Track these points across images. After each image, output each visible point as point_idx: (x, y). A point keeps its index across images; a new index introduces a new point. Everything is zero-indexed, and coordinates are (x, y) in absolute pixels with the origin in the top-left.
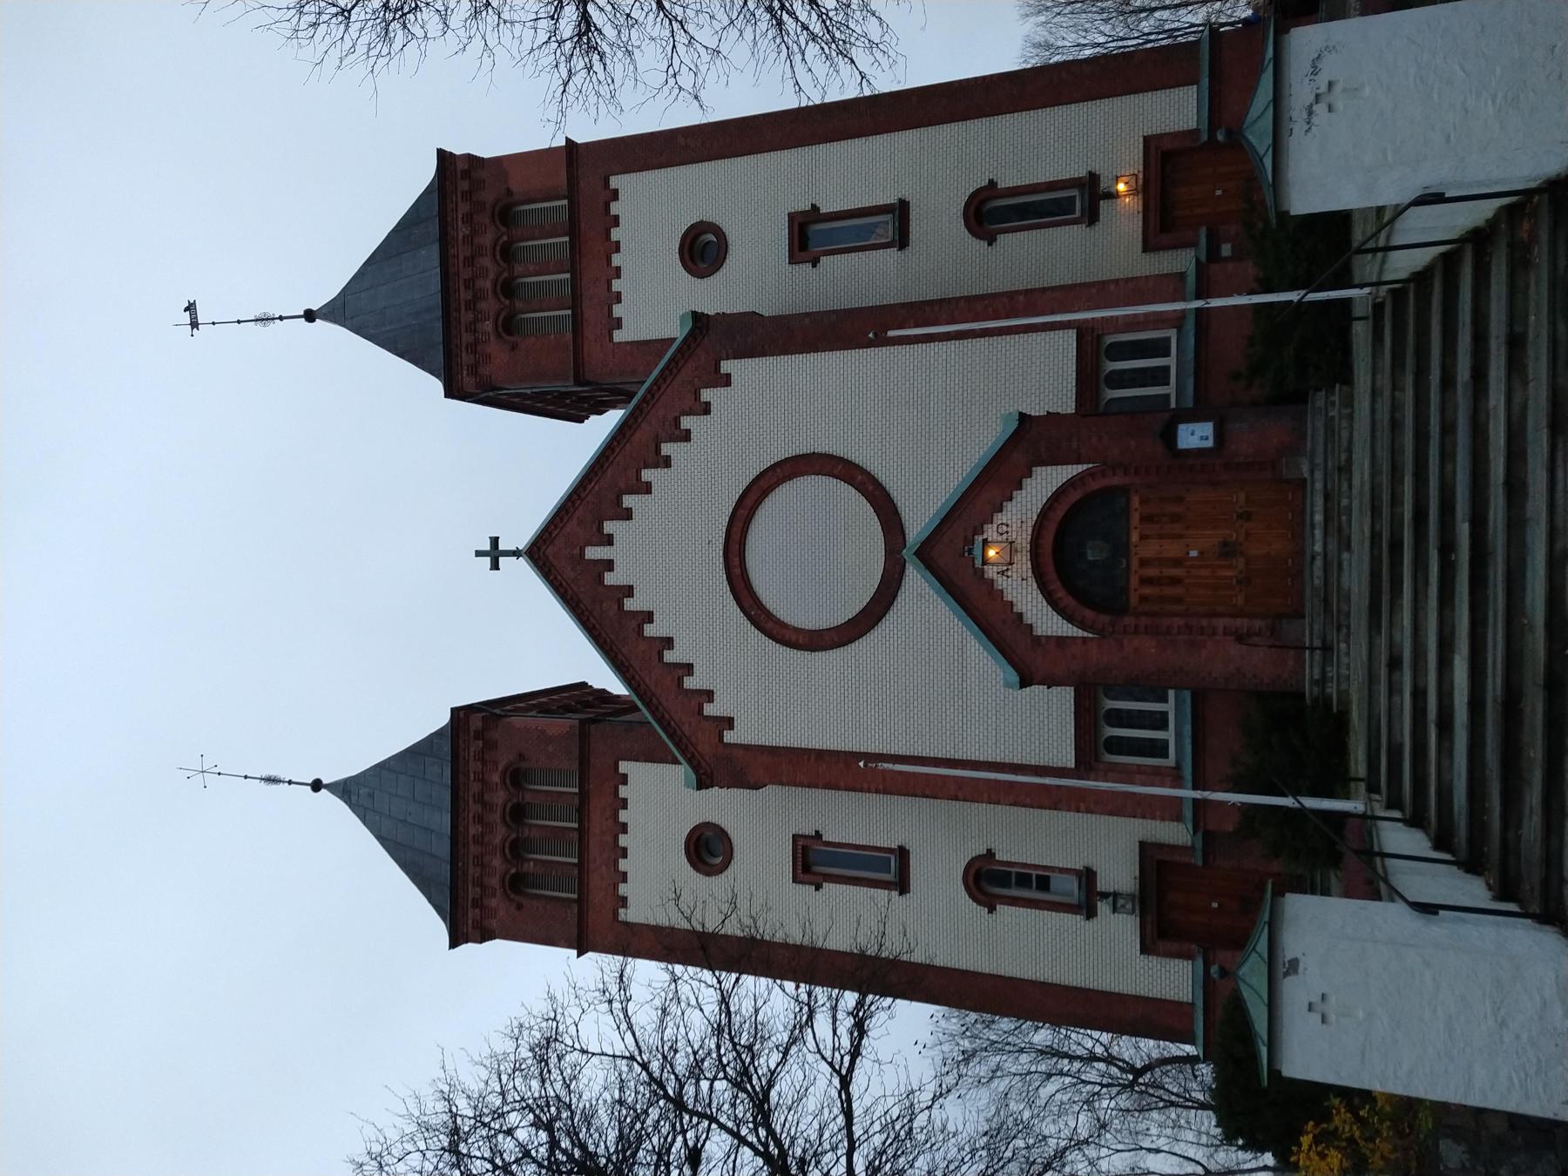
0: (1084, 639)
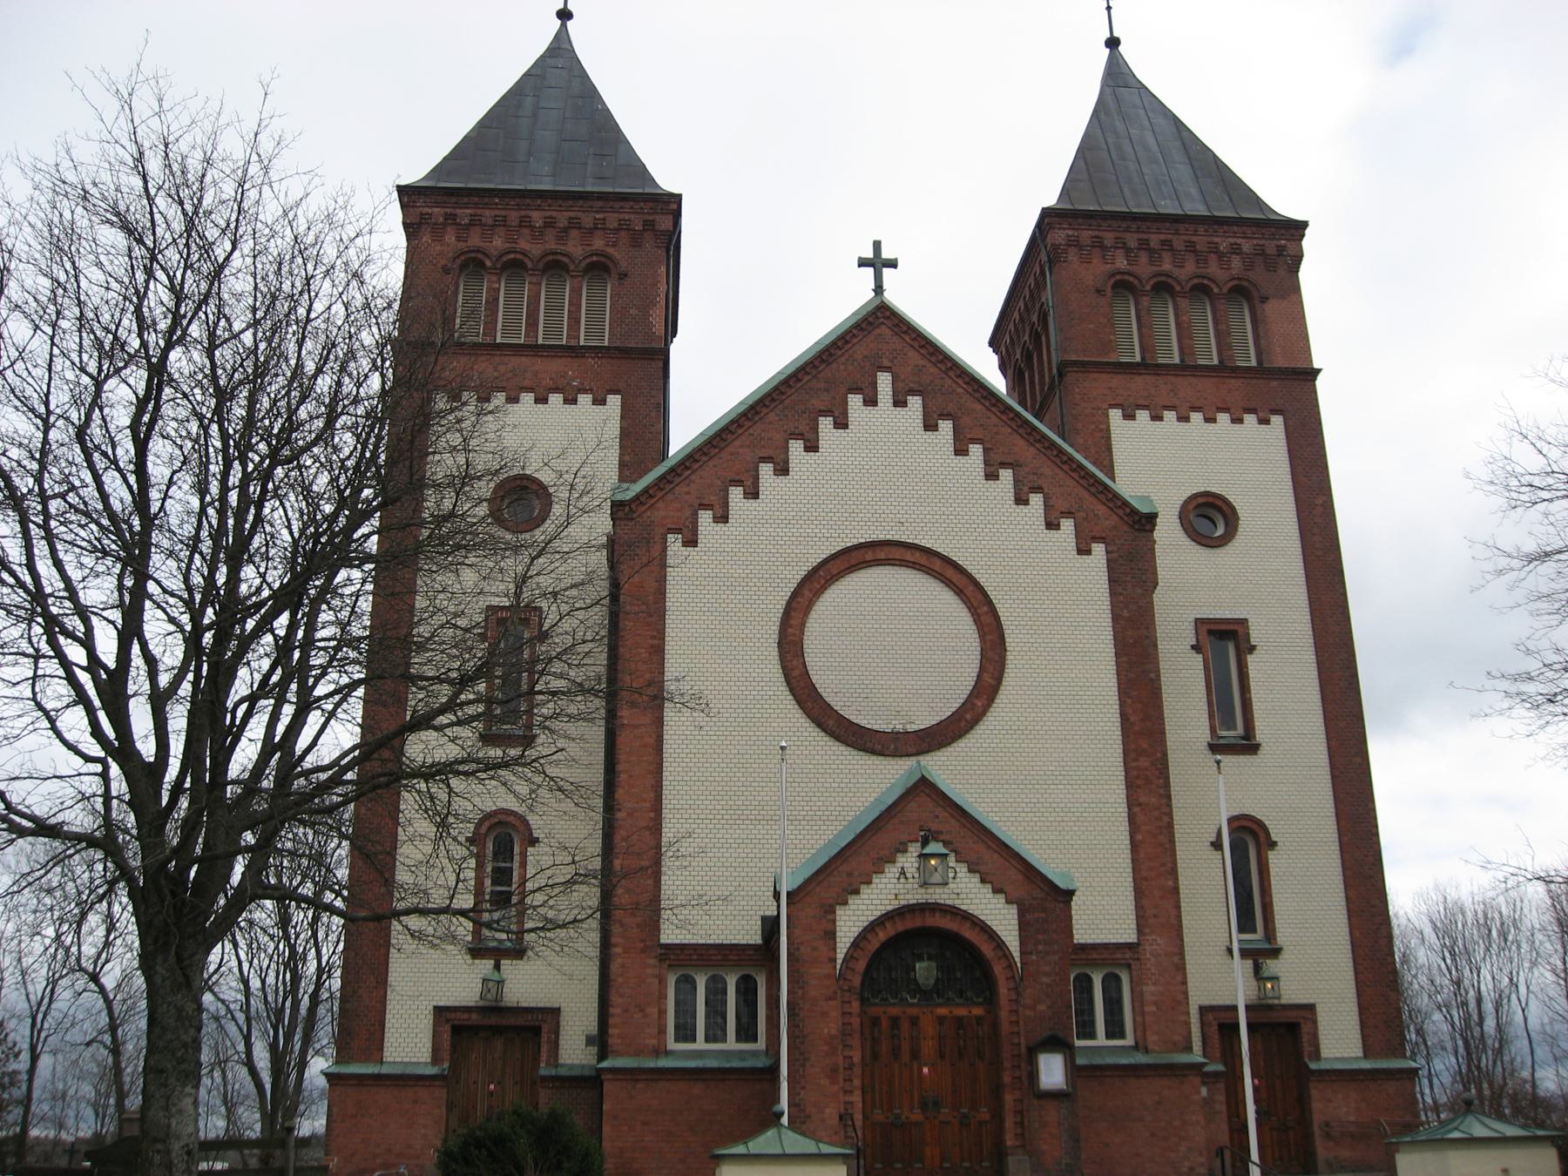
0: (835, 960)
